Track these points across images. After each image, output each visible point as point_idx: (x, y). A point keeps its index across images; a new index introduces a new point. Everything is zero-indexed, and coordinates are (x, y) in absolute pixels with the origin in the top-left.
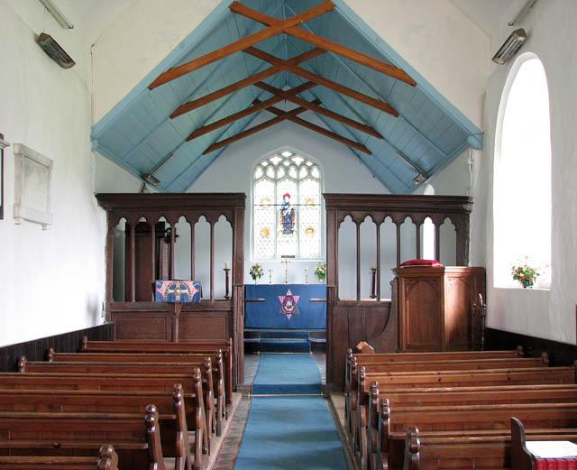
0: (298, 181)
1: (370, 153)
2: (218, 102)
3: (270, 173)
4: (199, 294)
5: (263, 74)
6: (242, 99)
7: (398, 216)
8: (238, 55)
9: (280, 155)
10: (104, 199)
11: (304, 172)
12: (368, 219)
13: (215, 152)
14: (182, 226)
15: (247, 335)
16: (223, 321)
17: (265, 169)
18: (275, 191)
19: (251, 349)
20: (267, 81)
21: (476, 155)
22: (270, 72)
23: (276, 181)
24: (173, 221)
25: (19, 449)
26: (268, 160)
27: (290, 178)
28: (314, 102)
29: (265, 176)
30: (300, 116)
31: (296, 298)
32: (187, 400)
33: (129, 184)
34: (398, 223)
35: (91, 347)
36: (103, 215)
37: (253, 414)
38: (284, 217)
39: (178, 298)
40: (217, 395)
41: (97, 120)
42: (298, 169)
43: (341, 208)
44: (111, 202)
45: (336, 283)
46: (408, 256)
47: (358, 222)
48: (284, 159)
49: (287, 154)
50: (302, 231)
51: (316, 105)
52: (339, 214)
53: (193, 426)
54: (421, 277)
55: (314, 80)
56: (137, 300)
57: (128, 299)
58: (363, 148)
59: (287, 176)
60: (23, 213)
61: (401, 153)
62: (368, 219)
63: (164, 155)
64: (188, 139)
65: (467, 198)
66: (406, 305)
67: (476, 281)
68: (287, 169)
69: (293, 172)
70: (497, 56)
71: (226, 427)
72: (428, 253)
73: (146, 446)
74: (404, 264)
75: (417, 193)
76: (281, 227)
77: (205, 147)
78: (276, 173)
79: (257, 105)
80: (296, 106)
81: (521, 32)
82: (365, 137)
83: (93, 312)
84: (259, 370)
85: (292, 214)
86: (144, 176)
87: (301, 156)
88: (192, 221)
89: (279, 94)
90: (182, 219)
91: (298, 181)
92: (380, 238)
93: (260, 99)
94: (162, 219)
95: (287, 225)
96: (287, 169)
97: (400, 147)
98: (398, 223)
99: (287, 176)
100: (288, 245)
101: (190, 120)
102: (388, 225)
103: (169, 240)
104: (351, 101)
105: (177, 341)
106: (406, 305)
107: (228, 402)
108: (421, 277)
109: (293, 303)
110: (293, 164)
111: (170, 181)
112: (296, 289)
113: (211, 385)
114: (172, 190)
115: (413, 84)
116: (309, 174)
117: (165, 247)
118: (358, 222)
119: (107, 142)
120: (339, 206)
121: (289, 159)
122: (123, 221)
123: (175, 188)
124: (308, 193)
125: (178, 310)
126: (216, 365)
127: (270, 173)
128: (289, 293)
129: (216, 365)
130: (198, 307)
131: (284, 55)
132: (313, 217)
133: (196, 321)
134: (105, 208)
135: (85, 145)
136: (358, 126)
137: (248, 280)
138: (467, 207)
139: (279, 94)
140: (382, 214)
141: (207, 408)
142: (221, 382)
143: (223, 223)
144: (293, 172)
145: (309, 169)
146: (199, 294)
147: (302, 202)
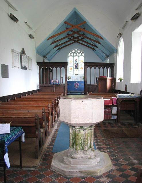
0: (79, 56)
1: (96, 50)
3: (72, 54)
4: (59, 83)
9: (74, 50)
10: (38, 63)
11: (80, 54)
12: (93, 67)
13: (58, 51)
17: (71, 53)
18: (73, 59)
21: (116, 54)
23: (73, 56)
24: (53, 68)
26: (72, 51)
27: (77, 56)
28: (82, 34)
29: (71, 55)
31: (78, 84)
33: (41, 61)
34: (99, 68)
35: (11, 102)
36: (38, 66)
38: (75, 65)
39: (55, 83)
41: (37, 47)
42: (79, 53)
45: (86, 80)
46: (101, 75)
47: (91, 68)
48: (76, 51)
49: (76, 50)
50: (80, 68)
52: (87, 67)
56: (45, 84)
59: (76, 55)
60: (14, 65)
61: (102, 51)
62: (93, 67)
63: (48, 52)
64: (54, 48)
65: (113, 63)
66: (100, 85)
67: (113, 80)
68: (76, 53)
69: (78, 54)
70: (118, 37)
74: (100, 77)
75: (104, 62)
76: (75, 67)
77: (57, 50)
78: (74, 55)
80: (78, 35)
82: (94, 47)
86: (44, 57)
87: (80, 50)
88: (57, 68)
89: (75, 38)
91: (79, 56)
92: (98, 72)
94: (50, 67)
95: (76, 66)
96: (76, 53)
97: (102, 50)
98: (99, 68)
99: (76, 55)
100: (76, 72)
101: (54, 45)
105: (54, 91)
106: (100, 85)
108: (103, 80)
109: (78, 85)
110: (78, 52)
112: (78, 82)
113: (50, 113)
115: (103, 39)
116: (82, 55)
118: (91, 68)
121: (77, 51)
124: (81, 59)
125: (55, 86)
126: (65, 94)
127: (72, 54)
128: (77, 83)
130: (58, 85)
132: (82, 65)
134: (38, 65)
136: (93, 45)
137: (68, 80)
140: (96, 66)
143: (63, 68)
144: (78, 54)
145: (82, 53)
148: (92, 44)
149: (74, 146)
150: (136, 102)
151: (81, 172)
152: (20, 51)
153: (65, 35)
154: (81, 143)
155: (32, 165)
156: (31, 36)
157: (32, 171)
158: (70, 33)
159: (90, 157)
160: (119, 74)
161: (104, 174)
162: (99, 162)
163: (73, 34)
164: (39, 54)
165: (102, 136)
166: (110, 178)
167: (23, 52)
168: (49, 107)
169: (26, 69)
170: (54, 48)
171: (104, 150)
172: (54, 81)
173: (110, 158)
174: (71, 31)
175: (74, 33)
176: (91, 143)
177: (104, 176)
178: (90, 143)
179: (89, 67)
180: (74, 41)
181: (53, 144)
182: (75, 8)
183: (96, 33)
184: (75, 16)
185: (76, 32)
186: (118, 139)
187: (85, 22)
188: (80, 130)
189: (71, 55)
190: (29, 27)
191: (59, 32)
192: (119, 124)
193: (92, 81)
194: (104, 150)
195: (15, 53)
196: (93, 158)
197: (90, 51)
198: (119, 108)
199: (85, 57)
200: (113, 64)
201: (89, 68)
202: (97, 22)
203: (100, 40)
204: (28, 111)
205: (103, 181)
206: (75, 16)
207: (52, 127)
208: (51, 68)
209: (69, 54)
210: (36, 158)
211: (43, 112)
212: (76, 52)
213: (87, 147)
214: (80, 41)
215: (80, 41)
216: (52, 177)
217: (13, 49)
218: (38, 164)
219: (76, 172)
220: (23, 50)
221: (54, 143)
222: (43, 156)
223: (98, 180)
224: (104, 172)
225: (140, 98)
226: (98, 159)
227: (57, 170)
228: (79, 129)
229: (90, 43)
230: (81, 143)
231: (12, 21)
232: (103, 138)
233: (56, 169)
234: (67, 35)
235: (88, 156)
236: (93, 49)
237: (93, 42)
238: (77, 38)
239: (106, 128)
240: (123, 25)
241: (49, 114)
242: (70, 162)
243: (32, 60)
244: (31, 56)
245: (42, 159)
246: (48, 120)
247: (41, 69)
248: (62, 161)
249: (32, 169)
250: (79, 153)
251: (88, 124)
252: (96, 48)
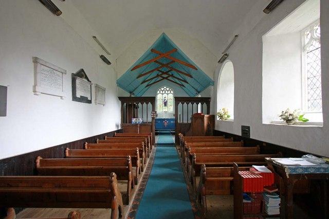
0: (168, 94)
2: (149, 74)
3: (161, 92)
5: (159, 68)
8: (153, 63)
10: (120, 98)
14: (140, 104)
15: (156, 130)
16: (150, 128)
19: (157, 134)
21: (212, 87)
22: (161, 67)
23: (163, 94)
25: (219, 72)
30: (168, 78)
32: (139, 151)
33: (127, 95)
36: (120, 102)
37: (157, 151)
40: (148, 147)
41: (119, 77)
44: (122, 99)
46: (195, 112)
47: (183, 104)
51: (172, 76)
54: (198, 117)
55: (172, 69)
57: (127, 123)
58: (183, 86)
67: (212, 118)
69: (167, 92)
70: (219, 61)
71: (151, 154)
72: (199, 112)
73: (110, 191)
79: (158, 76)
80: (167, 76)
81: (226, 55)
82: (183, 83)
83: (117, 126)
84: (159, 139)
86: (131, 93)
89: (163, 73)
90: (140, 103)
91: (168, 94)
95: (165, 103)
100: (165, 109)
103: (136, 108)
104: (181, 74)
107: (151, 148)
111: (137, 94)
114: (138, 96)
115: (197, 70)
117: (136, 110)
118: (183, 104)
119: (120, 84)
120: (178, 100)
122: (125, 104)
124: (170, 97)
125: (139, 126)
126: (148, 140)
127: (161, 92)
129: (148, 140)
131: (165, 63)
133: (143, 128)
136: (186, 74)
139: (163, 73)
141: (145, 152)
142: (144, 153)
144: (167, 92)
148: (180, 78)
153: (153, 65)
180: (162, 77)
182: (164, 33)
184: (164, 41)
185: (165, 63)
187: (176, 50)
189: (160, 93)
191: (147, 60)
193: (185, 120)
195: (39, 65)
197: (178, 88)
200: (209, 98)
202: (189, 49)
203: (192, 72)
206: (164, 41)
215: (170, 78)
217: (35, 56)
231: (106, 65)
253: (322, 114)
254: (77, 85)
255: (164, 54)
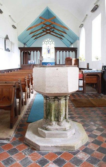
4: (35, 63)
6: (41, 31)
7: (66, 51)
10: (20, 48)
11: (51, 42)
13: (35, 40)
17: (45, 42)
20: (46, 28)
24: (31, 52)
30: (51, 33)
31: (50, 65)
33: (22, 46)
34: (66, 52)
36: (20, 51)
43: (57, 49)
46: (68, 57)
47: (60, 52)
50: (51, 53)
53: (29, 87)
58: (62, 39)
68: (48, 42)
69: (49, 42)
70: (80, 27)
76: (47, 52)
82: (62, 37)
85: (49, 50)
86: (24, 44)
88: (34, 52)
89: (47, 30)
93: (43, 27)
94: (29, 51)
96: (48, 42)
98: (66, 52)
100: (48, 55)
102: (64, 52)
115: (68, 30)
116: (52, 43)
118: (60, 52)
119: (20, 39)
120: (57, 49)
121: (49, 40)
123: (29, 46)
124: (52, 46)
125: (32, 65)
127: (45, 43)
128: (49, 64)
132: (53, 51)
135: (17, 39)
138: (77, 49)
143: (38, 52)
144: (49, 42)
146: (35, 63)
147: (51, 48)
148: (60, 34)
149: (48, 117)
150: (98, 76)
151: (56, 147)
152: (5, 37)
153: (40, 27)
154: (56, 113)
155: (5, 137)
156: (14, 27)
157: (4, 144)
158: (44, 30)
159: (66, 129)
160: (82, 54)
161: (81, 148)
162: (74, 134)
163: (46, 27)
164: (19, 41)
165: (73, 105)
166: (88, 153)
167: (7, 38)
168: (25, 80)
169: (9, 51)
170: (32, 38)
171: (77, 120)
172: (31, 61)
173: (84, 128)
174: (44, 24)
175: (47, 26)
176: (66, 114)
177: (81, 151)
178: (65, 113)
179: (58, 51)
180: (46, 32)
181: (29, 113)
182: (47, 7)
183: (63, 25)
185: (48, 25)
186: (87, 108)
187: (55, 17)
188: (55, 100)
190: (13, 20)
191: (37, 24)
192: (85, 95)
194: (77, 120)
196: (68, 130)
198: (85, 81)
199: (56, 44)
200: (76, 48)
201: (58, 52)
202: (64, 17)
203: (66, 31)
204: (6, 82)
205: (81, 157)
207: (28, 97)
208: (30, 52)
209: (43, 42)
210: (11, 127)
211: (19, 83)
212: (48, 41)
213: (62, 118)
214: (51, 33)
215: (51, 33)
216: (25, 152)
218: (12, 136)
219: (52, 146)
220: (7, 36)
221: (30, 112)
222: (18, 126)
223: (76, 156)
224: (80, 146)
225: (101, 72)
226: (74, 131)
227: (31, 144)
228: (54, 100)
229: (58, 33)
230: (56, 113)
232: (73, 108)
233: (30, 143)
234: (42, 31)
235: (63, 127)
236: (61, 38)
237: (60, 32)
238: (49, 30)
239: (74, 98)
240: (83, 18)
241: (25, 86)
242: (44, 134)
243: (15, 45)
244: (13, 42)
245: (17, 130)
246: (24, 91)
247: (22, 53)
248: (37, 133)
249: (5, 142)
250: (54, 125)
251: (63, 94)
252: (64, 34)
253: (23, 47)
254: (6, 43)
255: (47, 20)
